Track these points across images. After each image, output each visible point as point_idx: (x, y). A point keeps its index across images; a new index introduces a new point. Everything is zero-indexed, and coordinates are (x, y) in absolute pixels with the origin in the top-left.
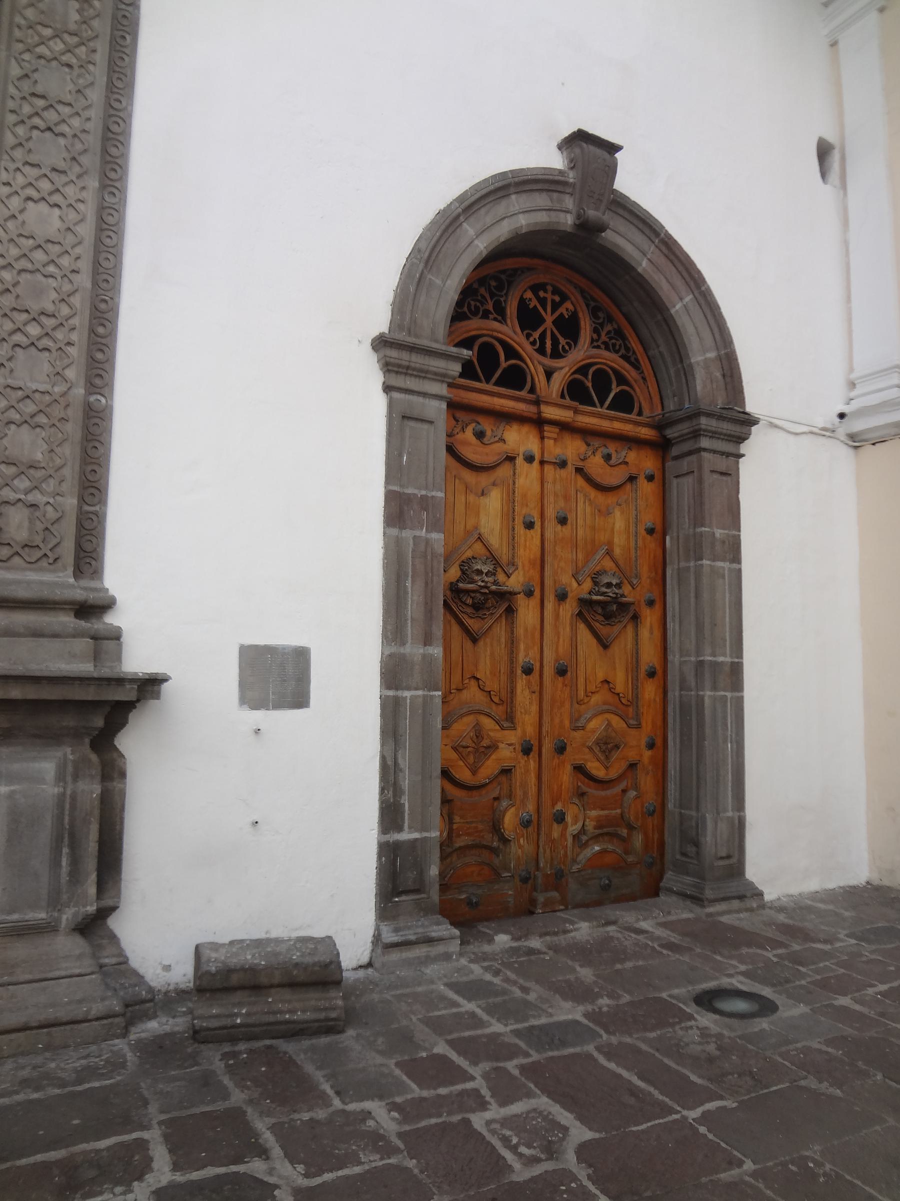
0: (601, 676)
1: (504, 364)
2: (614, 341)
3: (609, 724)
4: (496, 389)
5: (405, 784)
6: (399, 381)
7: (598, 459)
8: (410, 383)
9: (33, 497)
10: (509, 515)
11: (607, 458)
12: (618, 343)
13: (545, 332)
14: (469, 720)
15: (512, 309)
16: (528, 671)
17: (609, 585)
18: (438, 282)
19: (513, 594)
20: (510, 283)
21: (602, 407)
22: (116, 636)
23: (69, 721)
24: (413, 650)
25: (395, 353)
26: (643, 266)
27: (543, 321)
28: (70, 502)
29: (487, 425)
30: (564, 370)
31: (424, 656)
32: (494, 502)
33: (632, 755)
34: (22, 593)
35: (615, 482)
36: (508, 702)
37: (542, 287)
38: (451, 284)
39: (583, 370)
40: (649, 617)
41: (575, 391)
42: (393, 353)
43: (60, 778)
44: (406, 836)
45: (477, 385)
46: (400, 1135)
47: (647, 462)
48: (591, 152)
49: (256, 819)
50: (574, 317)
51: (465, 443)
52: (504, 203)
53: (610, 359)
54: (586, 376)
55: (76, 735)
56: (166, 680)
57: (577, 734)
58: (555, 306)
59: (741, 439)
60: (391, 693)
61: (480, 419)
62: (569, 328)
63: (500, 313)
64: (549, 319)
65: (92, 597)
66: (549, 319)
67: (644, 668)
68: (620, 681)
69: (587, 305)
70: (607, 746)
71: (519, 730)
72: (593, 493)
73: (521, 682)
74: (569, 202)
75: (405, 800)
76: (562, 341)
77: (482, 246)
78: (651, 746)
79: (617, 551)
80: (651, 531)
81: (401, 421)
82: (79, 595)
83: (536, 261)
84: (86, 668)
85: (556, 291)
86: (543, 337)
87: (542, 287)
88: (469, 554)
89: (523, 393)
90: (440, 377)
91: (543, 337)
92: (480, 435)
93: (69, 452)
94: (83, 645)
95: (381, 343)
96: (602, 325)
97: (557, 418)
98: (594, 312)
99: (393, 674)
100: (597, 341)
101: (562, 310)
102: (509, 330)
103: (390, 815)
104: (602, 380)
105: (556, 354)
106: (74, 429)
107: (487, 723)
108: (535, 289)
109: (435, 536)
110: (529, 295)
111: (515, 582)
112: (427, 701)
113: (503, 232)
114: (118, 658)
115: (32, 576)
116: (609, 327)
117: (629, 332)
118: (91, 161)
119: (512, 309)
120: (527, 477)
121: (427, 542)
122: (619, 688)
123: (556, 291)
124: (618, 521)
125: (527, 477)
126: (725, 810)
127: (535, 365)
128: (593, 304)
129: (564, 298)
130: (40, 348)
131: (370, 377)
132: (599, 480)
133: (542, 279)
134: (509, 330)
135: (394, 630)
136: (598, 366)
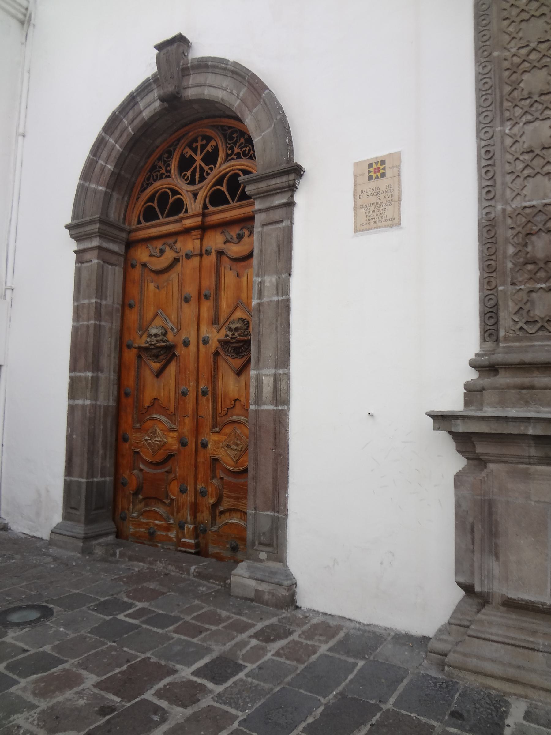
2: (244, 149)
12: (247, 149)
20: (174, 150)
25: (76, 229)
30: (204, 189)
42: (73, 232)
54: (173, 196)
56: (441, 419)
58: (203, 147)
59: (292, 188)
62: (211, 159)
64: (198, 159)
66: (198, 159)
67: (209, 396)
69: (225, 136)
80: (131, 306)
83: (187, 128)
97: (174, 230)
100: (231, 154)
108: (190, 146)
110: (188, 150)
127: (185, 189)
128: (171, 149)
129: (209, 139)
130: (544, 173)
131: (68, 247)
134: (177, 181)
136: (160, 191)
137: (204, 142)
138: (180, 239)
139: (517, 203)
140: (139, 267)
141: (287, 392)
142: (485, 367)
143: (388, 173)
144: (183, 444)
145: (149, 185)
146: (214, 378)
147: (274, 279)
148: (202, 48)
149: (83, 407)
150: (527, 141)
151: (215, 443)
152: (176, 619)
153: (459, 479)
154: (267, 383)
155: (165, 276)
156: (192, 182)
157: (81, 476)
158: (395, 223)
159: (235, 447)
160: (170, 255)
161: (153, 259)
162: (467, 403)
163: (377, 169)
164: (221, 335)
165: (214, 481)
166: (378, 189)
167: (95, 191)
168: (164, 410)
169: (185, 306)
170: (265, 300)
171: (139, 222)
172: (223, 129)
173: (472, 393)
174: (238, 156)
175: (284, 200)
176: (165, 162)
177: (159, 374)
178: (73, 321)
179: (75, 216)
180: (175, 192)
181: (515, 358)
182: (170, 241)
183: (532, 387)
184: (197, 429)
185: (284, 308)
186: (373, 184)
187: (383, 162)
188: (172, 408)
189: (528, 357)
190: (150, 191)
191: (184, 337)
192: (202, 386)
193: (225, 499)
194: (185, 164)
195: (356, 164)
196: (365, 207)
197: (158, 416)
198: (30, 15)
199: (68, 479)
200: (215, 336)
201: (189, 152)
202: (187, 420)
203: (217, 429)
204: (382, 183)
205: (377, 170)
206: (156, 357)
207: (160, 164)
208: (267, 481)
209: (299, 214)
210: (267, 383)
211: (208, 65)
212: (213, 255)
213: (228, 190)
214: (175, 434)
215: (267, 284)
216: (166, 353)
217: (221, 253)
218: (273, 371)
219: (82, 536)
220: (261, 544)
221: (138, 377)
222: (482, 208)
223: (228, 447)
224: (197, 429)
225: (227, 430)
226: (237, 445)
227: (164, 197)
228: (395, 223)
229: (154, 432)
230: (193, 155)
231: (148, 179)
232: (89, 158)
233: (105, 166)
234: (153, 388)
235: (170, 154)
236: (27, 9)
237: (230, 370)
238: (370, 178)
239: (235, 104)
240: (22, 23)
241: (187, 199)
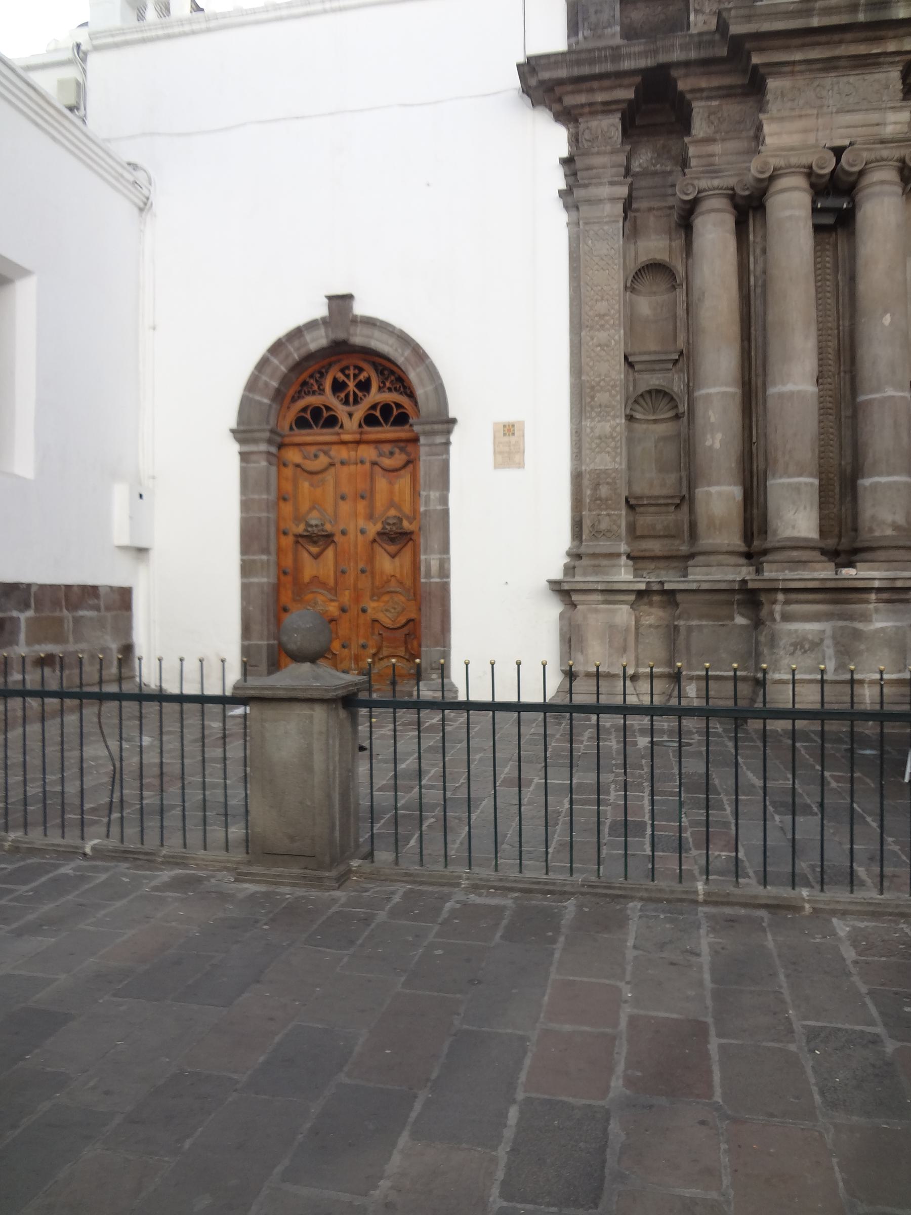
20: (327, 372)
21: (317, 425)
25: (241, 434)
27: (356, 386)
30: (360, 412)
39: (374, 407)
41: (370, 420)
46: (856, 962)
48: (340, 303)
49: (144, 496)
58: (355, 376)
59: (449, 432)
60: (445, 580)
62: (364, 386)
63: (322, 391)
66: (351, 385)
69: (376, 370)
76: (360, 394)
85: (356, 367)
86: (347, 396)
87: (348, 368)
89: (337, 429)
90: (613, 200)
91: (347, 396)
95: (233, 431)
104: (386, 409)
105: (356, 401)
108: (342, 371)
119: (328, 384)
123: (356, 367)
127: (341, 411)
128: (324, 370)
129: (361, 370)
131: (233, 449)
133: (344, 363)
138: (335, 447)
139: (592, 466)
140: (291, 467)
141: (449, 570)
142: (575, 555)
143: (516, 433)
144: (343, 610)
146: (371, 559)
147: (437, 494)
148: (360, 309)
149: (260, 585)
150: (597, 432)
151: (374, 608)
152: (15, 899)
153: (562, 616)
154: (435, 565)
155: (320, 476)
157: (261, 639)
158: (521, 465)
159: (393, 611)
160: (323, 460)
161: (307, 462)
162: (565, 574)
163: (509, 429)
164: (379, 527)
165: (374, 637)
166: (509, 442)
167: (260, 403)
168: (324, 585)
169: (341, 503)
170: (431, 507)
171: (291, 429)
172: (375, 365)
173: (569, 570)
174: (390, 390)
175: (444, 440)
176: (317, 381)
177: (316, 557)
178: (242, 511)
179: (240, 421)
180: (328, 408)
181: (591, 551)
182: (325, 448)
183: (599, 566)
184: (357, 599)
185: (445, 514)
186: (506, 439)
187: (513, 426)
188: (331, 582)
189: (598, 551)
190: (301, 403)
191: (341, 527)
192: (361, 565)
193: (384, 649)
194: (338, 387)
195: (495, 424)
196: (501, 453)
197: (319, 590)
198: (152, 204)
199: (246, 643)
200: (373, 529)
201: (341, 377)
202: (347, 593)
203: (375, 598)
204: (513, 439)
205: (509, 430)
206: (315, 543)
207: (312, 381)
208: (437, 627)
210: (435, 565)
211: (370, 322)
212: (368, 465)
213: (381, 415)
214: (336, 604)
215: (432, 497)
216: (320, 539)
217: (374, 463)
218: (439, 556)
220: (432, 669)
221: (296, 560)
222: (573, 465)
223: (387, 610)
224: (357, 599)
225: (386, 598)
226: (395, 609)
227: (316, 412)
228: (521, 465)
229: (316, 603)
230: (346, 380)
231: (300, 392)
232: (253, 373)
233: (620, 566)
234: (309, 569)
235: (322, 375)
236: (148, 199)
237: (385, 555)
238: (505, 435)
239: (400, 360)
240: (141, 210)
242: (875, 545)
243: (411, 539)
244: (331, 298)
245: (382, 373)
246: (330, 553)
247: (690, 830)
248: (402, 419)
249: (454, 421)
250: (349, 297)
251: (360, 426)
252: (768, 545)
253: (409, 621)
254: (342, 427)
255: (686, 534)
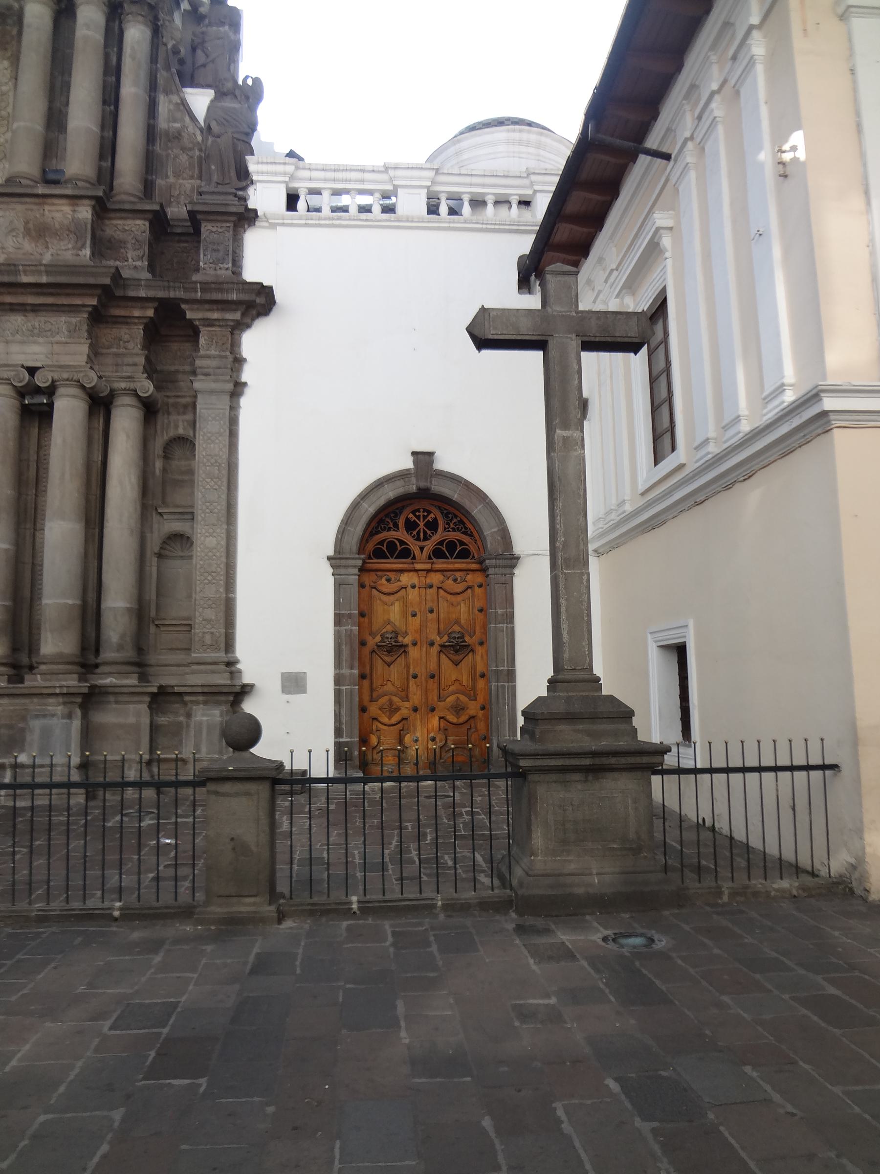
0: (454, 678)
1: (399, 548)
3: (458, 698)
4: (396, 561)
5: (344, 721)
6: (339, 571)
7: (450, 581)
8: (343, 571)
9: (212, 630)
10: (404, 612)
11: (455, 580)
13: (419, 531)
14: (387, 697)
15: (401, 522)
16: (415, 677)
17: (454, 638)
18: (352, 529)
19: (406, 646)
20: (401, 513)
22: (240, 672)
23: (223, 698)
24: (346, 671)
25: (336, 561)
26: (455, 497)
28: (223, 631)
29: (392, 575)
30: (429, 545)
31: (351, 674)
32: (397, 607)
33: (472, 712)
34: (209, 660)
35: (459, 590)
36: (406, 689)
37: (418, 510)
38: (358, 529)
39: (441, 543)
40: (480, 650)
41: (437, 553)
42: (333, 562)
43: (221, 715)
44: (344, 739)
45: (388, 561)
47: (479, 578)
48: (424, 459)
50: (435, 519)
51: (382, 585)
52: (381, 490)
53: (453, 536)
55: (226, 702)
57: (442, 704)
58: (425, 517)
59: (514, 566)
61: (388, 573)
62: (433, 526)
63: (396, 526)
64: (421, 524)
65: (232, 660)
66: (421, 524)
68: (465, 680)
69: (442, 513)
70: (458, 709)
71: (411, 703)
72: (449, 597)
73: (412, 682)
74: (414, 480)
75: (344, 727)
76: (429, 532)
77: (372, 510)
78: (483, 708)
79: (463, 622)
81: (339, 586)
82: (226, 660)
84: (228, 682)
85: (425, 510)
88: (385, 630)
89: (409, 560)
90: (355, 566)
91: (419, 532)
92: (388, 581)
93: (222, 615)
94: (227, 675)
96: (451, 521)
98: (446, 516)
99: (338, 680)
101: (429, 518)
102: (401, 534)
103: (338, 732)
104: (451, 546)
105: (426, 538)
106: (223, 607)
107: (395, 699)
108: (414, 512)
109: (354, 628)
110: (411, 515)
111: (407, 640)
112: (351, 691)
113: (382, 501)
114: (240, 678)
115: (213, 655)
116: (455, 520)
117: (465, 520)
118: (223, 519)
119: (401, 522)
120: (413, 595)
121: (351, 630)
122: (465, 683)
123: (425, 510)
124: (463, 608)
125: (413, 595)
126: (505, 736)
129: (429, 512)
131: (327, 570)
132: (451, 591)
134: (401, 534)
135: (338, 664)
137: (426, 514)
145: (378, 533)
148: (443, 463)
156: (418, 539)
174: (454, 530)
176: (392, 520)
209: (517, 581)
212: (435, 588)
219: (842, 439)
227: (391, 546)
231: (377, 528)
235: (396, 515)
241: (417, 552)
242: (45, 661)
243: (404, 651)
244: (414, 454)
245: (446, 515)
246: (401, 661)
247: (388, 944)
248: (465, 554)
249: (517, 558)
250: (431, 454)
251: (430, 558)
252: (99, 661)
253: (403, 719)
254: (414, 558)
255: (223, 645)
